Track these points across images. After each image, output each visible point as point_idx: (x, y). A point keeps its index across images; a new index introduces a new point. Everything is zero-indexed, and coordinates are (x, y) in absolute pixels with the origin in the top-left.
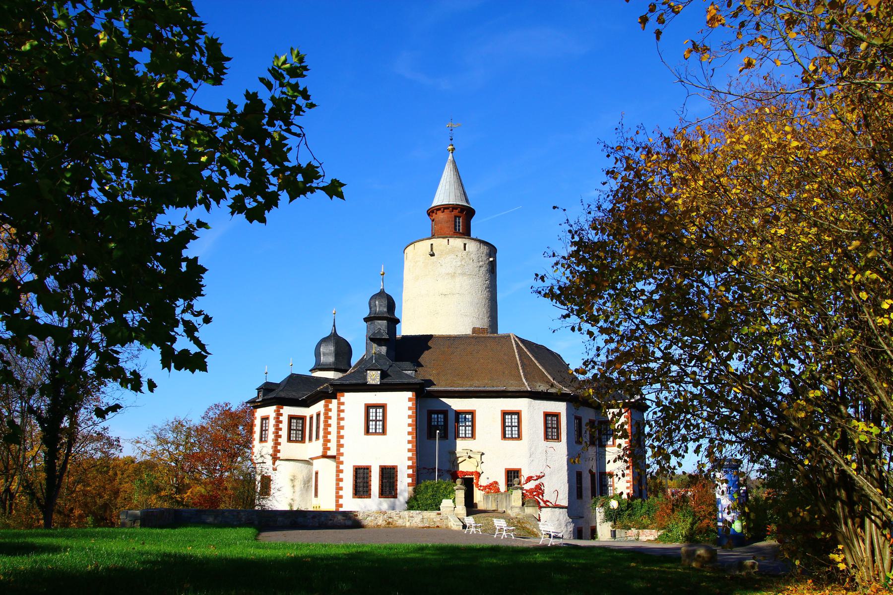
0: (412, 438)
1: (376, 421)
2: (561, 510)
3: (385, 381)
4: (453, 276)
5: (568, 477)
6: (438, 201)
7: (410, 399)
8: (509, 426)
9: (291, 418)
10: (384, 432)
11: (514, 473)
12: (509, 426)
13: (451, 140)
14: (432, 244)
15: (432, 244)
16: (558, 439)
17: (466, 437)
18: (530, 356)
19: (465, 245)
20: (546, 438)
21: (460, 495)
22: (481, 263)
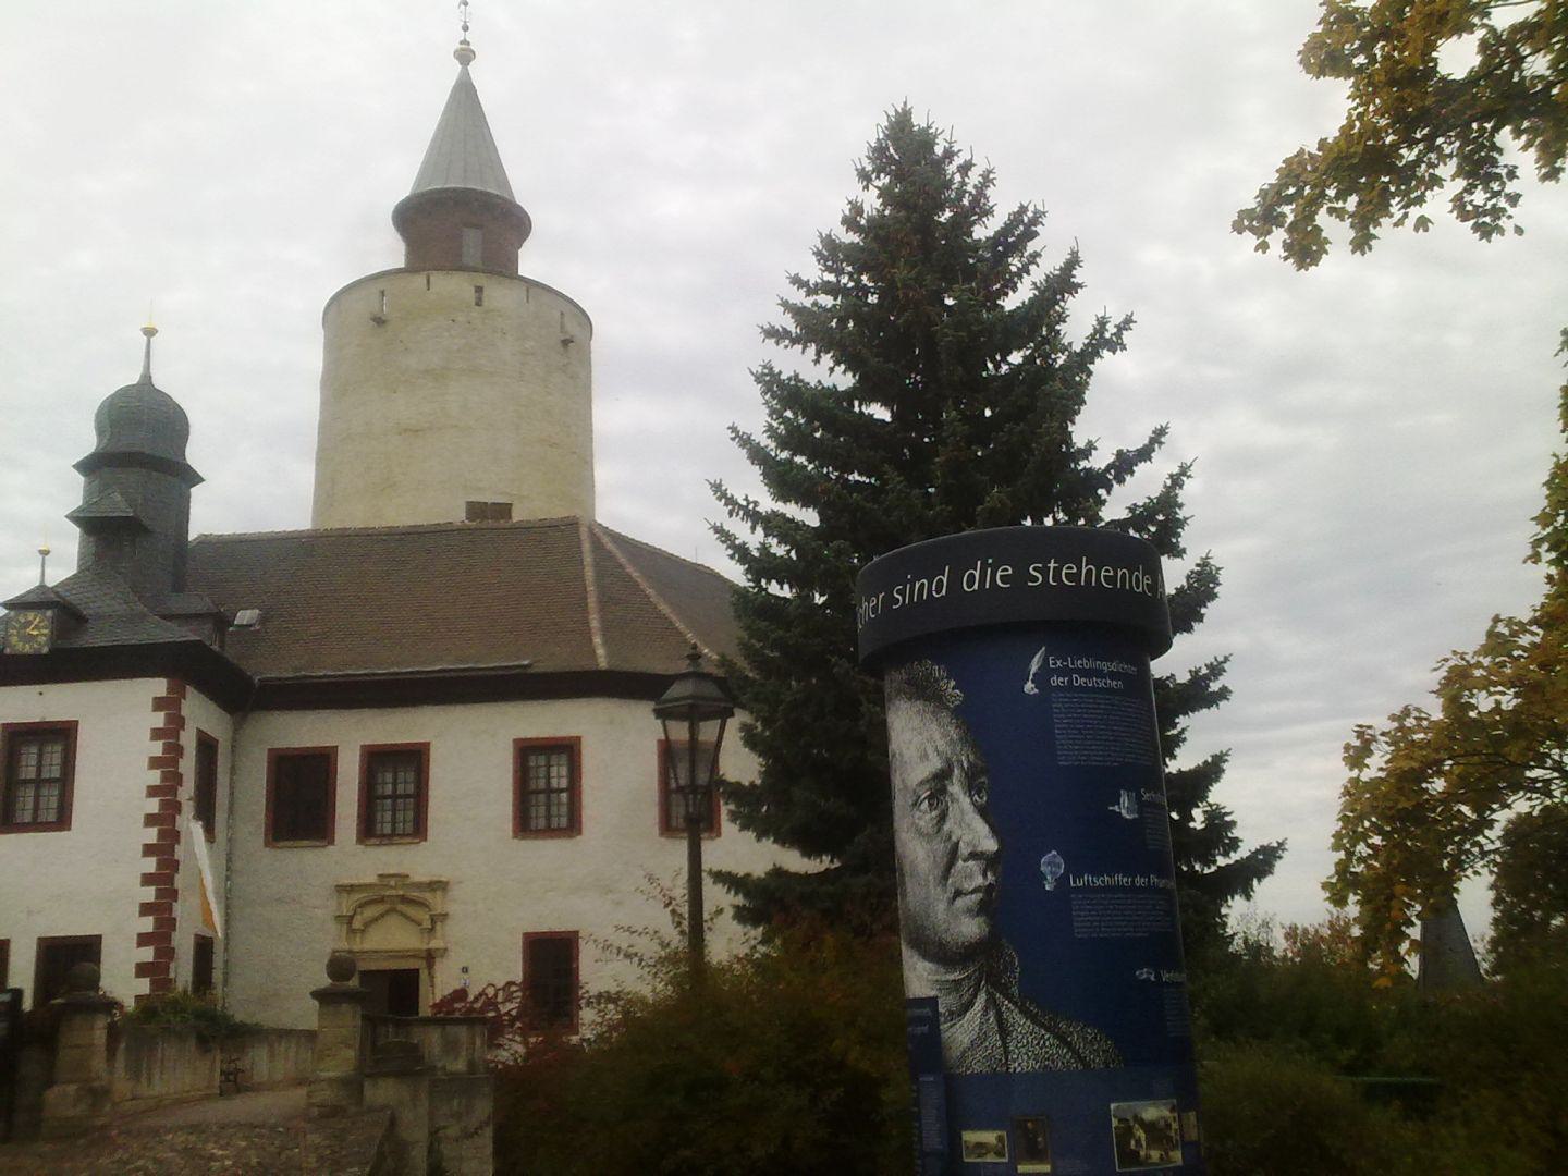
9: (377, 759)
10: (62, 821)
17: (393, 834)
19: (479, 290)
22: (529, 344)
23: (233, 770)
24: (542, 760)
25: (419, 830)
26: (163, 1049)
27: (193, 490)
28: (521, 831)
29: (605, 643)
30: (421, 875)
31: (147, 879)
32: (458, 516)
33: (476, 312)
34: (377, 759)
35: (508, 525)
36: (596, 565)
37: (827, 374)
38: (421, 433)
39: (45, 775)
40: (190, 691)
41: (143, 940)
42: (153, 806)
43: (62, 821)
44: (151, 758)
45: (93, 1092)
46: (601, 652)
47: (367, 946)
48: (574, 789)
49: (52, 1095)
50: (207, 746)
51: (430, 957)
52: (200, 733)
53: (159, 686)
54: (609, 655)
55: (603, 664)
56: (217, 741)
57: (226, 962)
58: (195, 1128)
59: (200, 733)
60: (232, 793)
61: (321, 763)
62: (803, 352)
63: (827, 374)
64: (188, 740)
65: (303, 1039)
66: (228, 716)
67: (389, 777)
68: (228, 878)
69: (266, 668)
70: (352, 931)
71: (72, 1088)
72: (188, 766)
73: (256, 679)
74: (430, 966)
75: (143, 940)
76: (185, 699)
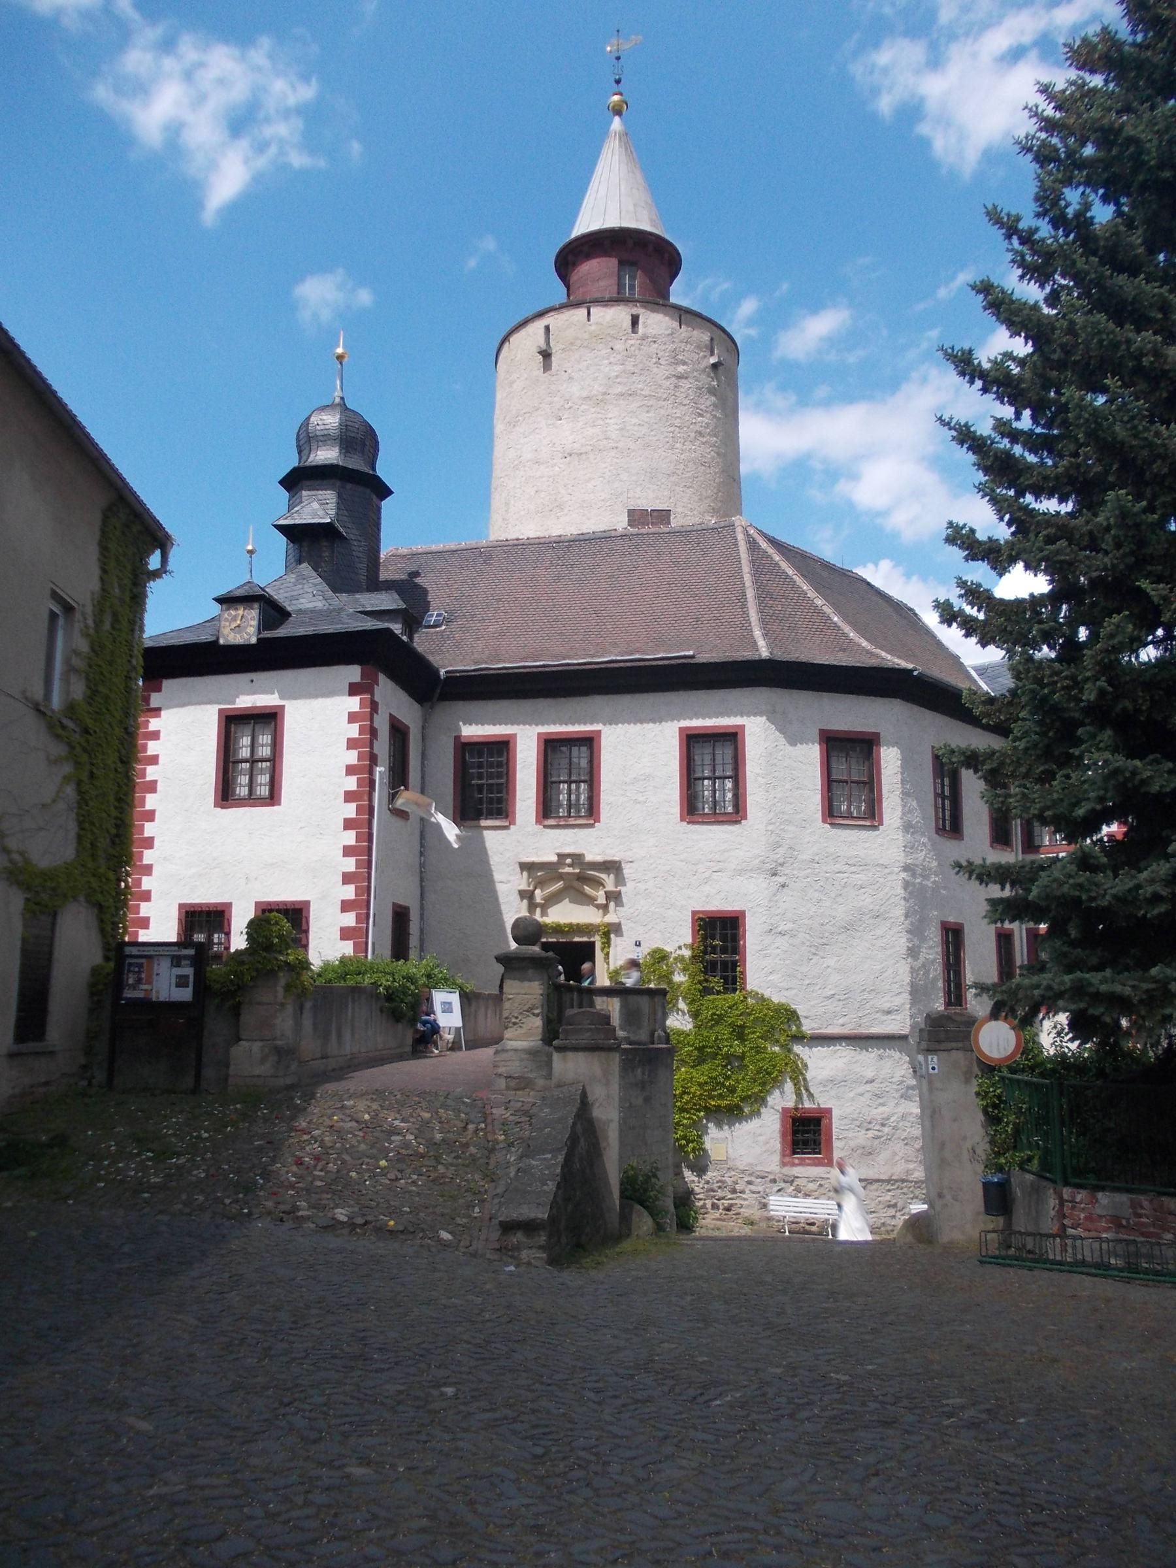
0: (143, 802)
1: (253, 761)
2: (723, 324)
3: (267, 634)
4: (600, 401)
5: (581, 204)
6: (588, 222)
7: (352, 717)
8: (246, 761)
10: (273, 798)
11: (724, 928)
12: (246, 761)
13: (618, 82)
14: (547, 328)
15: (547, 328)
16: (872, 815)
18: (790, 572)
19: (635, 321)
20: (830, 813)
21: (293, 1226)
22: (681, 369)
23: (424, 756)
24: (708, 750)
25: (592, 811)
26: (353, 1008)
27: (383, 503)
28: (187, 912)
29: (765, 636)
30: (593, 855)
31: (348, 851)
32: (620, 523)
33: (634, 341)
34: (551, 746)
35: (667, 530)
36: (753, 562)
37: (966, 446)
38: (584, 456)
39: (717, 774)
40: (382, 678)
41: (346, 906)
42: (351, 783)
43: (273, 798)
44: (349, 740)
45: (278, 1051)
46: (761, 642)
47: (548, 920)
48: (275, 759)
49: (239, 1051)
50: (398, 732)
51: (610, 931)
52: (392, 718)
53: (353, 673)
54: (769, 645)
55: (765, 653)
56: (409, 728)
57: (422, 931)
58: (378, 1094)
59: (392, 718)
60: (423, 778)
61: (502, 748)
62: (985, 206)
63: (966, 446)
64: (382, 724)
65: (490, 1002)
66: (416, 706)
67: (246, 741)
68: (421, 854)
69: (447, 663)
70: (532, 906)
71: (256, 1047)
72: (382, 747)
73: (442, 672)
74: (607, 943)
75: (346, 906)
76: (378, 685)
